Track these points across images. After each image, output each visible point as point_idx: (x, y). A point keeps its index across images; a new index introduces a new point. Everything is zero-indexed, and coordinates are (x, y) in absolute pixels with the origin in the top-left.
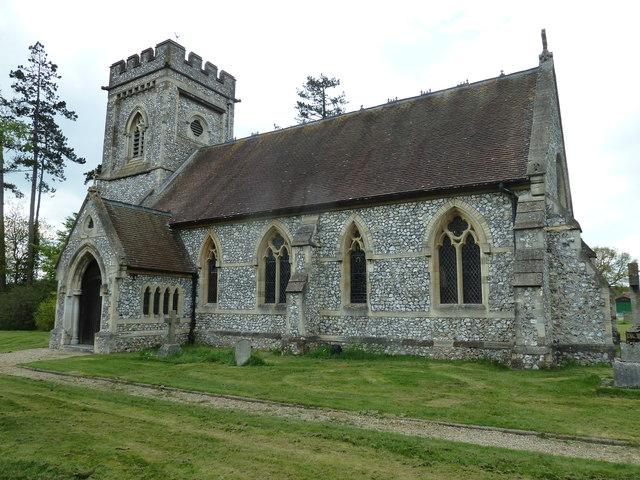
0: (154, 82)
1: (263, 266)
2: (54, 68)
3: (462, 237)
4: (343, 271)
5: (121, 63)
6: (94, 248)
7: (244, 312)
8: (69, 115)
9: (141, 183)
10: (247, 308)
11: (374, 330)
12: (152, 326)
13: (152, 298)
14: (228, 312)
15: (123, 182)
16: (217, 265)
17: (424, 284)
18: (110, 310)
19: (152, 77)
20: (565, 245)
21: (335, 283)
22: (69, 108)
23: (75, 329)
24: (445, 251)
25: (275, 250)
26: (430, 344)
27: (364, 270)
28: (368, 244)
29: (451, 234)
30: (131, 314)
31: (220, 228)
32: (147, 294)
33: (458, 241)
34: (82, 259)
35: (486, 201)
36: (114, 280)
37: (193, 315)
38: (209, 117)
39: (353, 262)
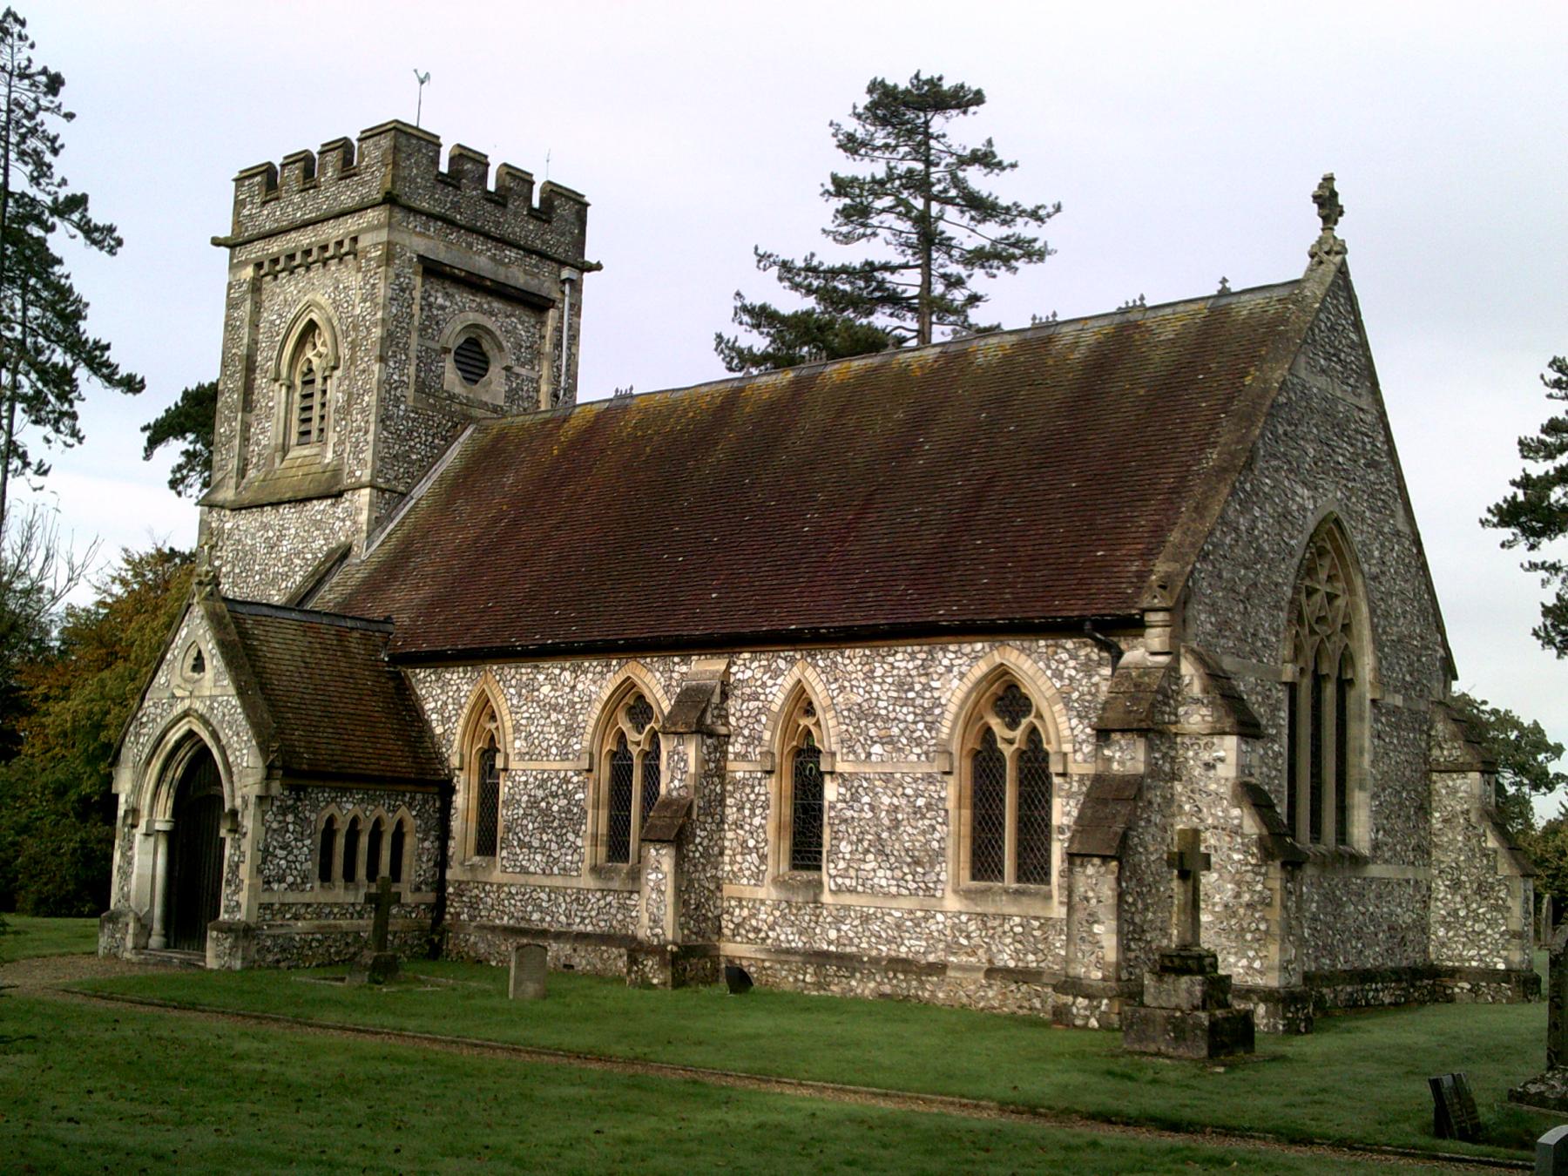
0: (355, 240)
1: (604, 771)
2: (55, 83)
3: (1018, 734)
4: (774, 792)
5: (268, 171)
6: (206, 722)
7: (559, 882)
8: (102, 237)
9: (317, 524)
10: (565, 871)
11: (833, 934)
12: (345, 910)
13: (340, 843)
14: (522, 879)
15: (269, 515)
16: (499, 764)
17: (937, 835)
18: (245, 871)
19: (351, 224)
20: (1209, 766)
21: (757, 821)
22: (98, 214)
23: (158, 911)
24: (985, 762)
25: (632, 736)
26: (939, 969)
27: (819, 794)
28: (830, 733)
29: (996, 724)
30: (290, 879)
31: (509, 671)
32: (329, 833)
33: (1011, 742)
34: (178, 745)
35: (1065, 656)
36: (253, 799)
37: (441, 885)
38: (501, 321)
39: (799, 772)
